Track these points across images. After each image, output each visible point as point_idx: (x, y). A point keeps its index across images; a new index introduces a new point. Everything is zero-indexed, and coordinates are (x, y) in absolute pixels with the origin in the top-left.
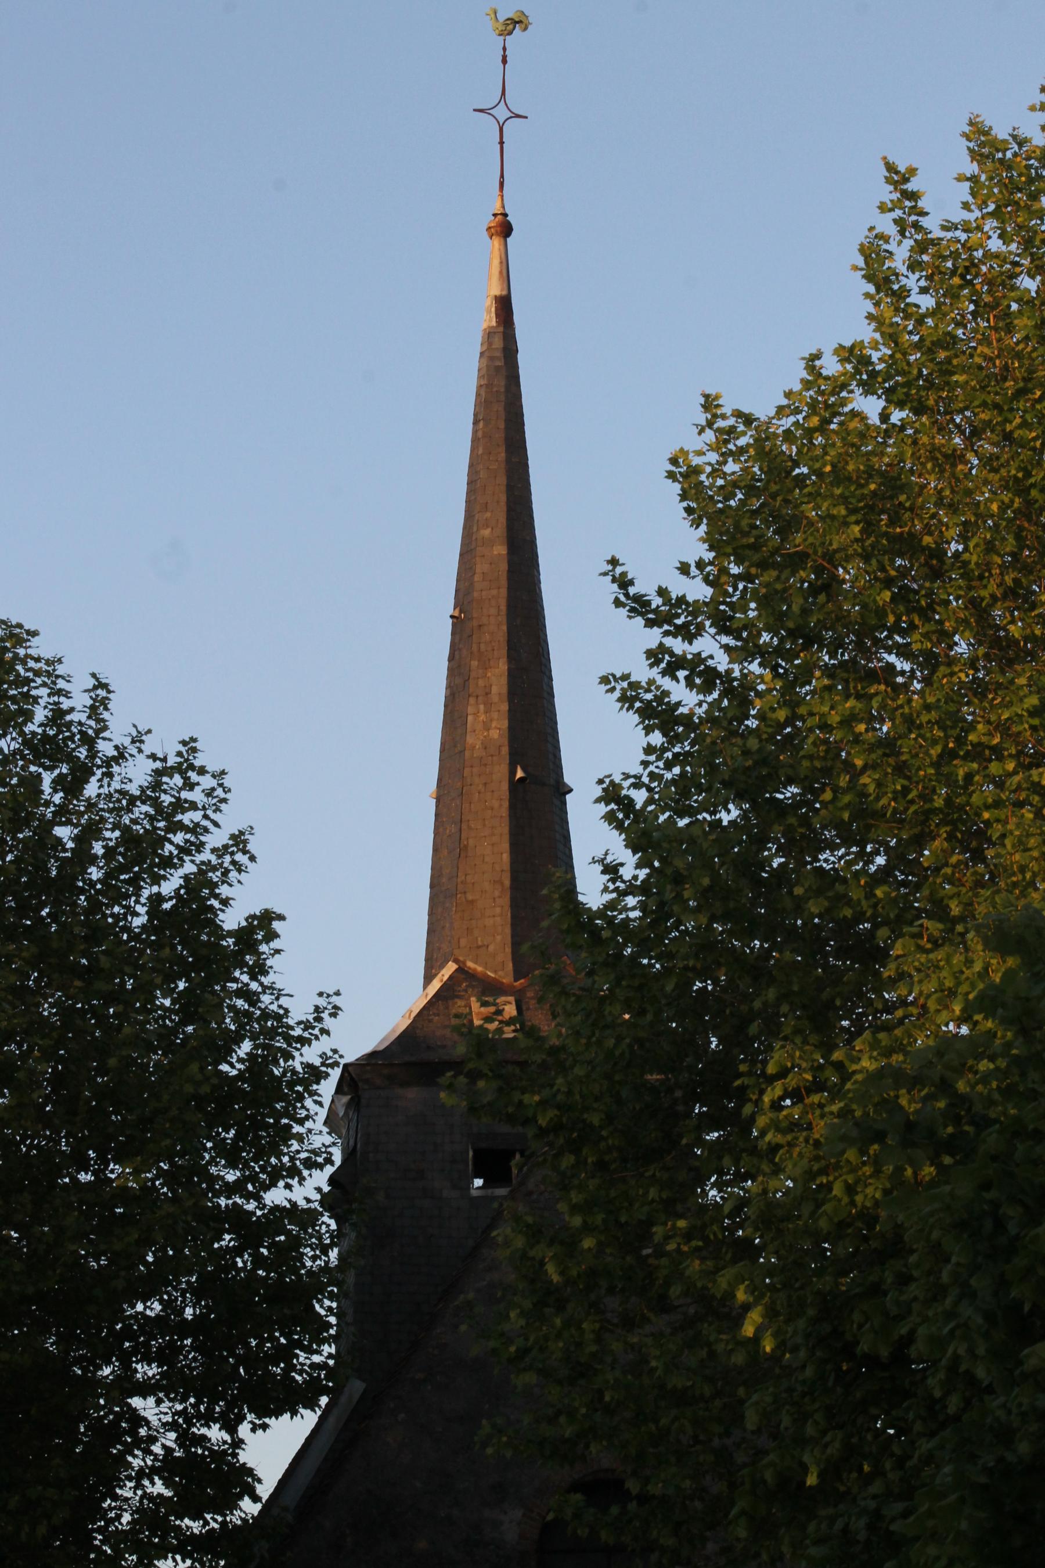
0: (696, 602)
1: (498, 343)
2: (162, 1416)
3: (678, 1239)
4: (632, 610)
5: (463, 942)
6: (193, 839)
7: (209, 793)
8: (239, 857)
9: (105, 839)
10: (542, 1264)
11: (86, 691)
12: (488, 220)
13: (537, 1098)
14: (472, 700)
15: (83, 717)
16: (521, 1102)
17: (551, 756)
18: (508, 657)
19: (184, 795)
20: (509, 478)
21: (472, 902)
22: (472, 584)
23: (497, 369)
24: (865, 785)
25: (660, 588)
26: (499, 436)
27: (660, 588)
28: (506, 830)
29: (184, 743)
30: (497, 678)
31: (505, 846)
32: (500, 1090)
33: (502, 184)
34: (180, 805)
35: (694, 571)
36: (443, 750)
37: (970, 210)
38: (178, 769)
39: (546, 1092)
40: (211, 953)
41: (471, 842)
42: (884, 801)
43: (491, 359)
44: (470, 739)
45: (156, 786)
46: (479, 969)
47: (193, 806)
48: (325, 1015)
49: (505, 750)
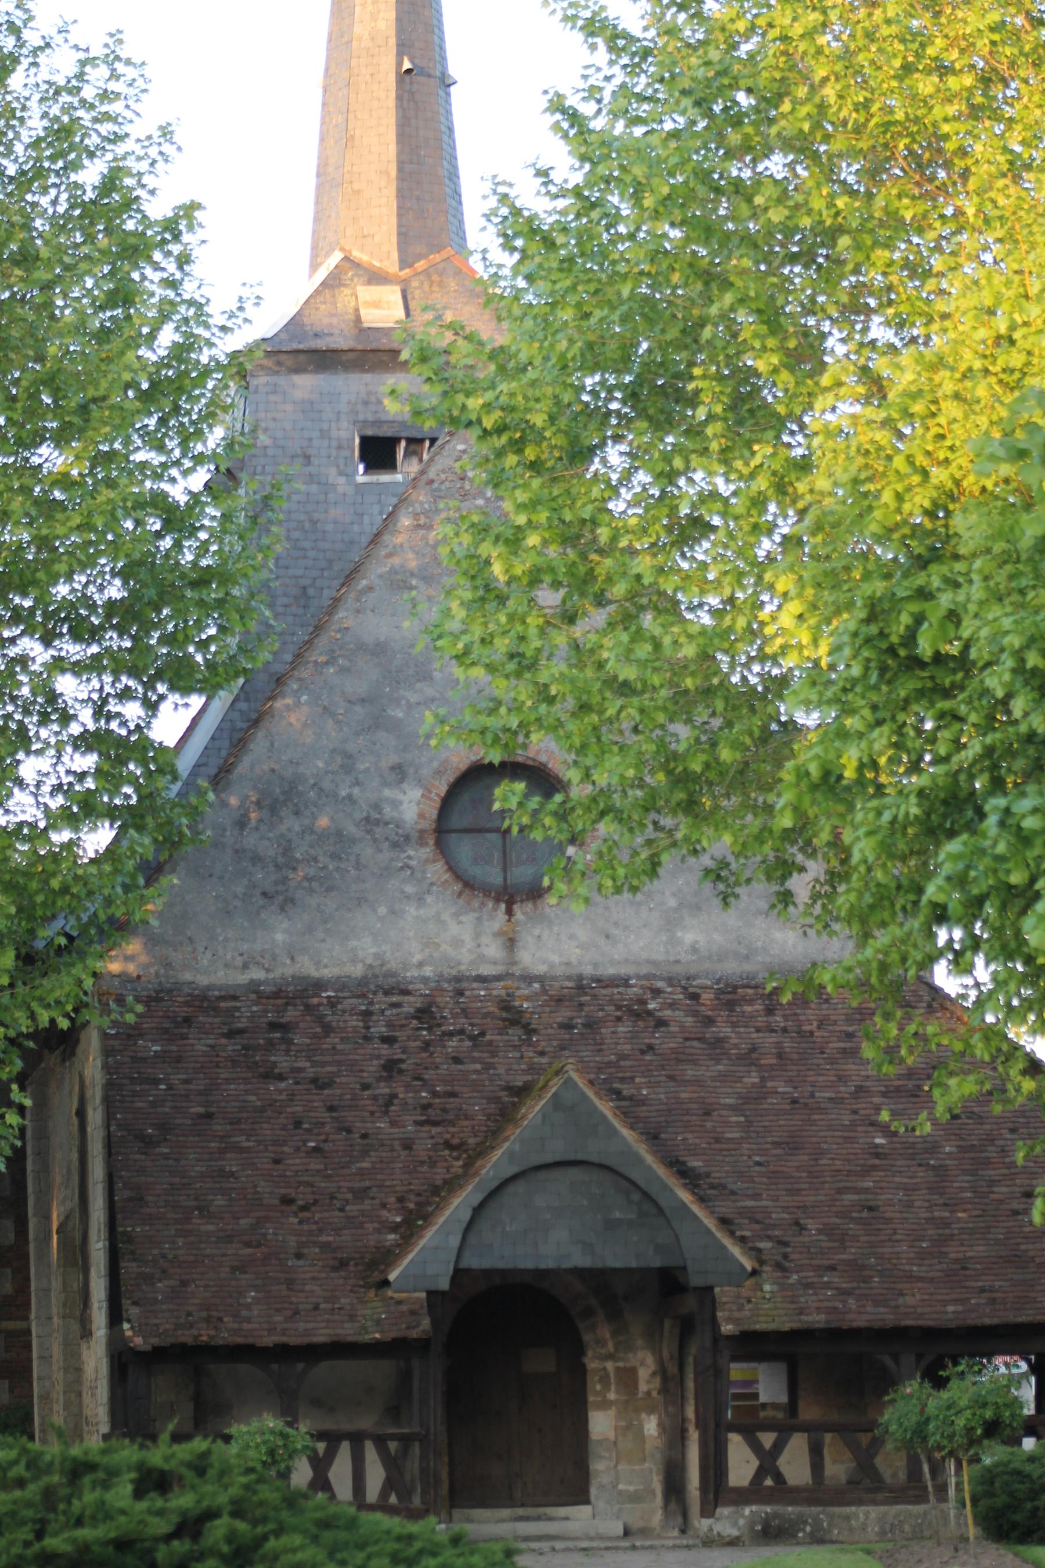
5: (349, 231)
8: (166, 148)
10: (488, 562)
13: (481, 401)
16: (464, 406)
19: (112, 86)
21: (358, 192)
31: (392, 136)
32: (445, 393)
39: (490, 396)
41: (358, 133)
44: (357, 29)
45: (80, 76)
49: (393, 41)
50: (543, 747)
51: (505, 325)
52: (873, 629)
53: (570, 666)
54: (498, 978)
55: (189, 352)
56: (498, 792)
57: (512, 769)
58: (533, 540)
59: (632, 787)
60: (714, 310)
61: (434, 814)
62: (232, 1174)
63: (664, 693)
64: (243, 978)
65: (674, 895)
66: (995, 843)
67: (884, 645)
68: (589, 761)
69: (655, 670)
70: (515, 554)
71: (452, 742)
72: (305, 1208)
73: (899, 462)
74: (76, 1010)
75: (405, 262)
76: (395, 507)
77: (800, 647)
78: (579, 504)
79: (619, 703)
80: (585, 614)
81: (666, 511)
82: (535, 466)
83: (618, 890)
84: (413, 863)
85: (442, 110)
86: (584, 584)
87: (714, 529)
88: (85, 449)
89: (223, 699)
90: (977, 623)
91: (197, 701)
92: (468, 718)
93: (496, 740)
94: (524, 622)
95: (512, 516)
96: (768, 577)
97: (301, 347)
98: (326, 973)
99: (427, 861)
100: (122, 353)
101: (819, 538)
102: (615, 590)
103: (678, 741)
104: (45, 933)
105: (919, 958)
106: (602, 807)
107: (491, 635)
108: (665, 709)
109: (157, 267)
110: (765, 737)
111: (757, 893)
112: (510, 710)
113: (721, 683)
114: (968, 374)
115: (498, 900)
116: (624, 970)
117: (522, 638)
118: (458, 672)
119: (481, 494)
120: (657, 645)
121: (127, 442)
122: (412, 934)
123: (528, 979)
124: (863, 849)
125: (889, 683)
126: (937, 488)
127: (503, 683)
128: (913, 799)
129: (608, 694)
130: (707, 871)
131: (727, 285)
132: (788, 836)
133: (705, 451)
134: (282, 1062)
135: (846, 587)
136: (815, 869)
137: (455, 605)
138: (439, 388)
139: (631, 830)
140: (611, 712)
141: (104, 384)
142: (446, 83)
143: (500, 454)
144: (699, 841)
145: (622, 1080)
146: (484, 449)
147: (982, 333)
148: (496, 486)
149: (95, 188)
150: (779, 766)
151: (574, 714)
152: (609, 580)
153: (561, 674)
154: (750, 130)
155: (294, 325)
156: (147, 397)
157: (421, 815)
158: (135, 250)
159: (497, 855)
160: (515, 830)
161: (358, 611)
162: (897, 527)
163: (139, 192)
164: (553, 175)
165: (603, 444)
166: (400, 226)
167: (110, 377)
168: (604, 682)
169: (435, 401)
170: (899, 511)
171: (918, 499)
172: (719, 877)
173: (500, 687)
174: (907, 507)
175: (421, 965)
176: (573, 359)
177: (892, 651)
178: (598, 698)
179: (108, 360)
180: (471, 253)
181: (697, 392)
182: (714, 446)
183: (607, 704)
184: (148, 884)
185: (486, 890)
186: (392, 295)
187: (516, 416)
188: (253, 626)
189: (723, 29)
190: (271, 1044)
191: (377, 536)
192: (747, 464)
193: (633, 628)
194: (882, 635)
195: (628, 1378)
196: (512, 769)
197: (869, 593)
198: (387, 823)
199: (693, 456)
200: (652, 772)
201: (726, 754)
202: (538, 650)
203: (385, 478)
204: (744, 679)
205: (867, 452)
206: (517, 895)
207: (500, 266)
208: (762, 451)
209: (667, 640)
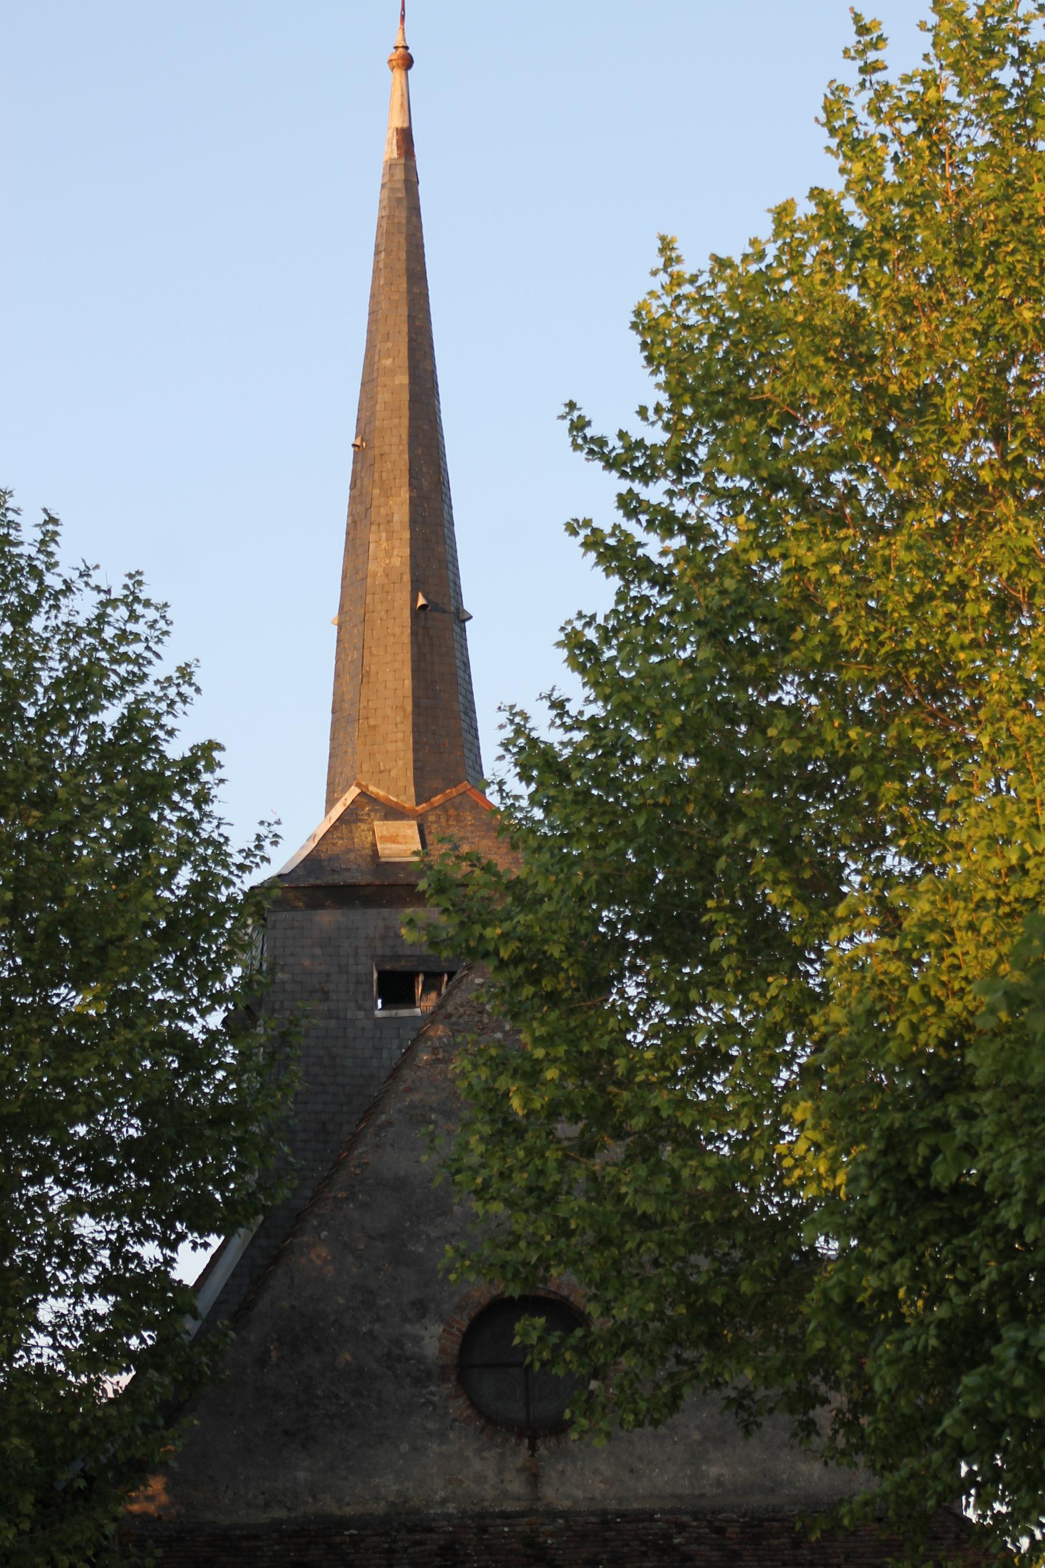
0: (654, 446)
1: (399, 174)
2: (96, 1235)
3: (646, 1071)
4: (591, 452)
6: (136, 670)
7: (152, 625)
8: (185, 689)
9: (52, 669)
10: (506, 1095)
11: (37, 525)
12: (389, 52)
13: (499, 931)
14: (374, 528)
15: (33, 551)
16: (481, 936)
17: (452, 585)
18: (410, 485)
19: (130, 627)
20: (410, 308)
21: (375, 727)
22: (374, 413)
23: (399, 200)
24: (838, 627)
25: (621, 431)
26: (401, 266)
27: (621, 431)
28: (408, 656)
29: (130, 576)
30: (399, 506)
31: (407, 672)
32: (462, 924)
33: (403, 17)
34: (123, 636)
35: (651, 413)
36: (344, 578)
37: (930, 62)
38: (124, 601)
39: (507, 926)
40: (149, 781)
42: (855, 644)
43: (393, 190)
44: (372, 567)
46: (382, 793)
47: (137, 637)
48: (266, 844)
49: (407, 578)
50: (562, 1280)
51: (521, 855)
52: (892, 1160)
53: (590, 1200)
54: (522, 1514)
55: (206, 891)
56: (518, 1327)
57: (533, 1304)
58: (551, 1074)
59: (653, 1320)
60: (726, 840)
61: (455, 1349)
63: (683, 1226)
64: (264, 1518)
65: (698, 1428)
66: (1013, 1373)
67: (902, 1177)
68: (610, 1295)
69: (673, 1203)
70: (533, 1086)
71: (472, 1277)
73: (914, 993)
74: (95, 1555)
75: (421, 797)
76: (414, 1041)
77: (819, 1177)
78: (596, 1035)
79: (638, 1236)
80: (604, 1147)
81: (683, 1041)
82: (552, 998)
83: (639, 1424)
84: (435, 1399)
85: (457, 646)
86: (603, 1117)
87: (732, 1059)
88: (103, 990)
89: (238, 1243)
90: (992, 1155)
91: (215, 1241)
92: (486, 1252)
93: (516, 1274)
94: (543, 1156)
95: (529, 1048)
96: (786, 1108)
97: (319, 882)
98: (349, 1510)
100: (140, 893)
101: (836, 1070)
102: (633, 1122)
103: (699, 1272)
104: (64, 1477)
105: (940, 1488)
106: (623, 1340)
107: (511, 1169)
108: (684, 1243)
109: (175, 807)
110: (787, 1267)
111: (778, 1425)
112: (529, 1244)
113: (741, 1215)
114: (982, 904)
115: (520, 1436)
117: (541, 1172)
118: (477, 1206)
119: (500, 1028)
120: (676, 1177)
121: (145, 981)
122: (434, 1471)
123: (552, 1514)
124: (883, 1379)
125: (906, 1214)
126: (952, 1018)
127: (522, 1218)
128: (933, 1331)
129: (628, 1228)
130: (730, 1401)
131: (740, 816)
132: (815, 1363)
133: (721, 985)
135: (863, 1118)
136: (839, 1399)
137: (473, 1140)
138: (456, 919)
139: (652, 1363)
140: (630, 1245)
141: (122, 924)
142: (461, 618)
143: (516, 986)
144: (721, 1374)
146: (501, 980)
147: (996, 863)
148: (515, 1017)
149: (113, 729)
150: (800, 1298)
151: (593, 1248)
152: (629, 1113)
153: (580, 1208)
154: (764, 661)
155: (311, 863)
156: (166, 939)
157: (443, 1351)
158: (155, 789)
160: (537, 1366)
161: (377, 1146)
162: (912, 1056)
163: (158, 732)
164: (568, 706)
165: (620, 978)
166: (415, 761)
167: (128, 917)
168: (624, 1215)
169: (452, 932)
170: (914, 1042)
171: (933, 1030)
172: (741, 1406)
173: (520, 1222)
174: (922, 1037)
175: (444, 1501)
176: (590, 891)
177: (910, 1182)
178: (618, 1232)
179: (125, 901)
180: (488, 784)
181: (712, 924)
182: (730, 978)
183: (626, 1237)
184: (169, 1423)
186: (409, 830)
187: (534, 947)
188: (272, 1163)
189: (737, 561)
191: (397, 1069)
192: (763, 995)
193: (653, 1160)
194: (900, 1166)
196: (533, 1304)
197: (886, 1124)
198: (408, 1359)
199: (710, 988)
200: (674, 1304)
201: (746, 1287)
202: (557, 1184)
203: (404, 1013)
204: (764, 1210)
205: (882, 983)
206: (541, 1430)
207: (517, 798)
208: (776, 984)
209: (685, 1173)
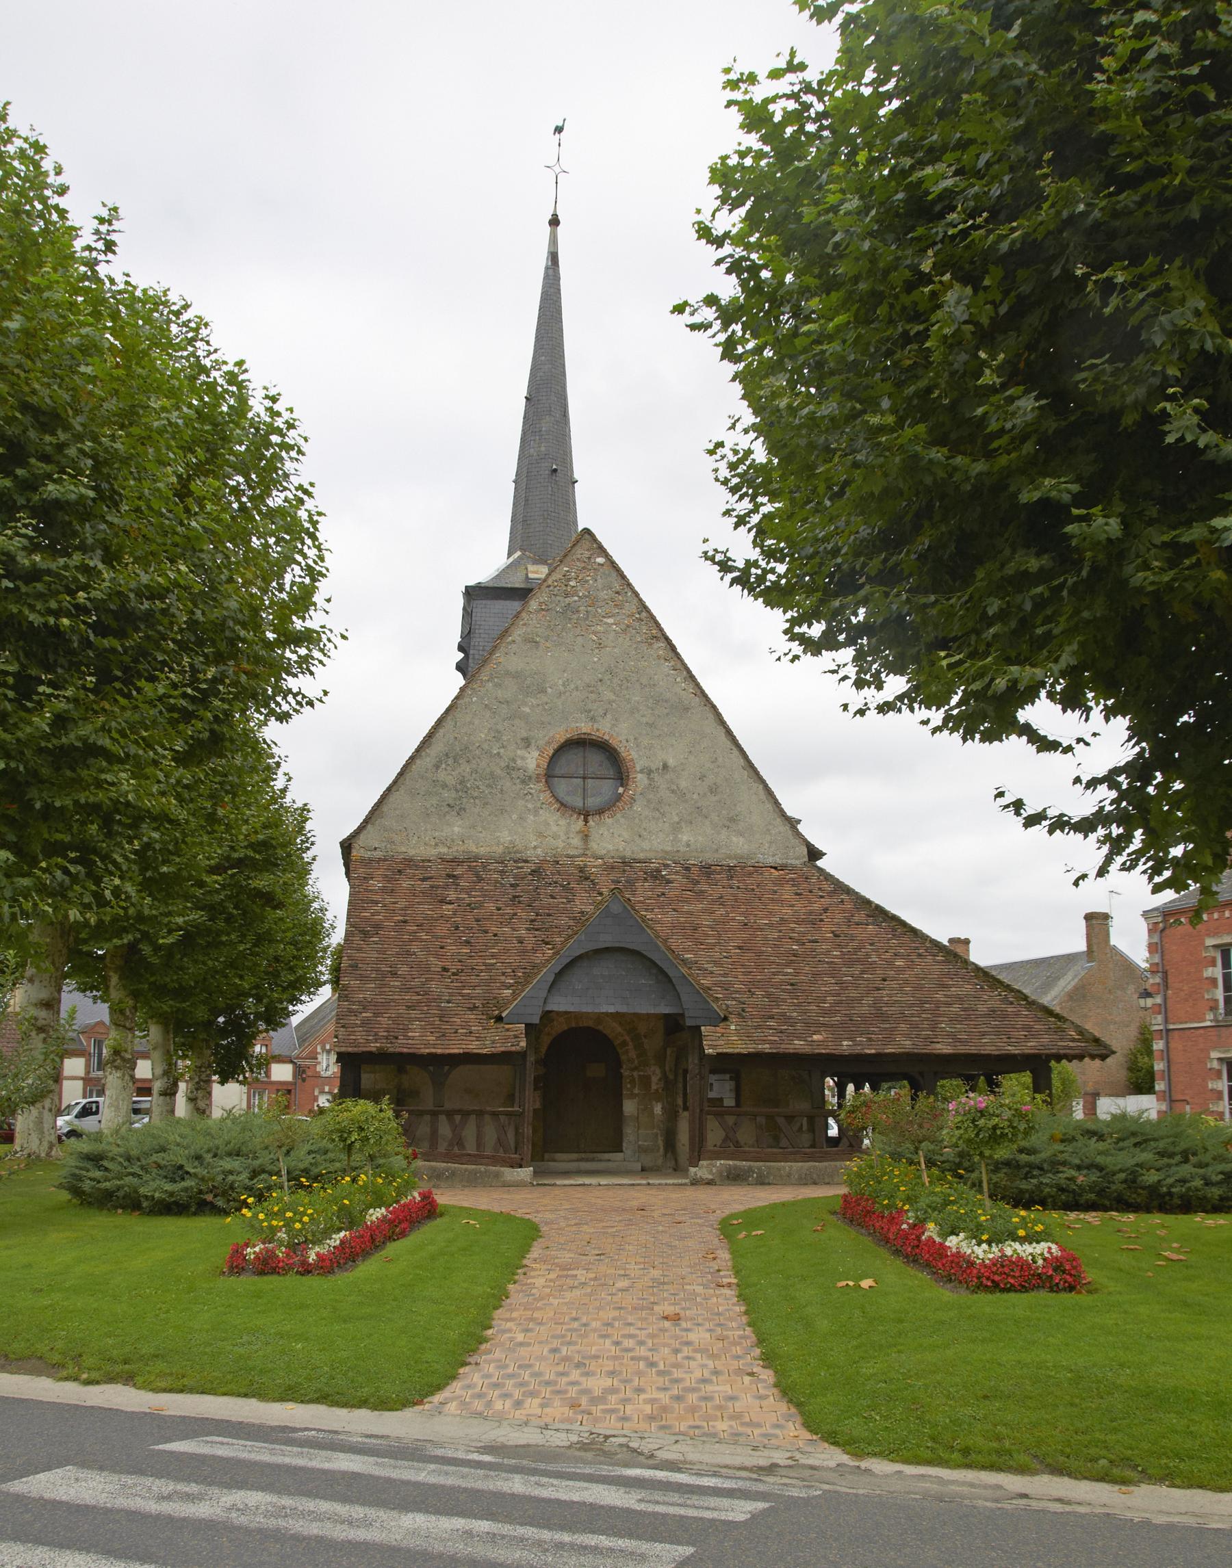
62: (414, 953)
64: (434, 852)
72: (454, 974)
99: (540, 791)
116: (649, 855)
134: (452, 895)
145: (646, 910)
157: (538, 766)
159: (580, 791)
175: (535, 848)
185: (573, 809)
190: (446, 887)
195: (646, 1081)
